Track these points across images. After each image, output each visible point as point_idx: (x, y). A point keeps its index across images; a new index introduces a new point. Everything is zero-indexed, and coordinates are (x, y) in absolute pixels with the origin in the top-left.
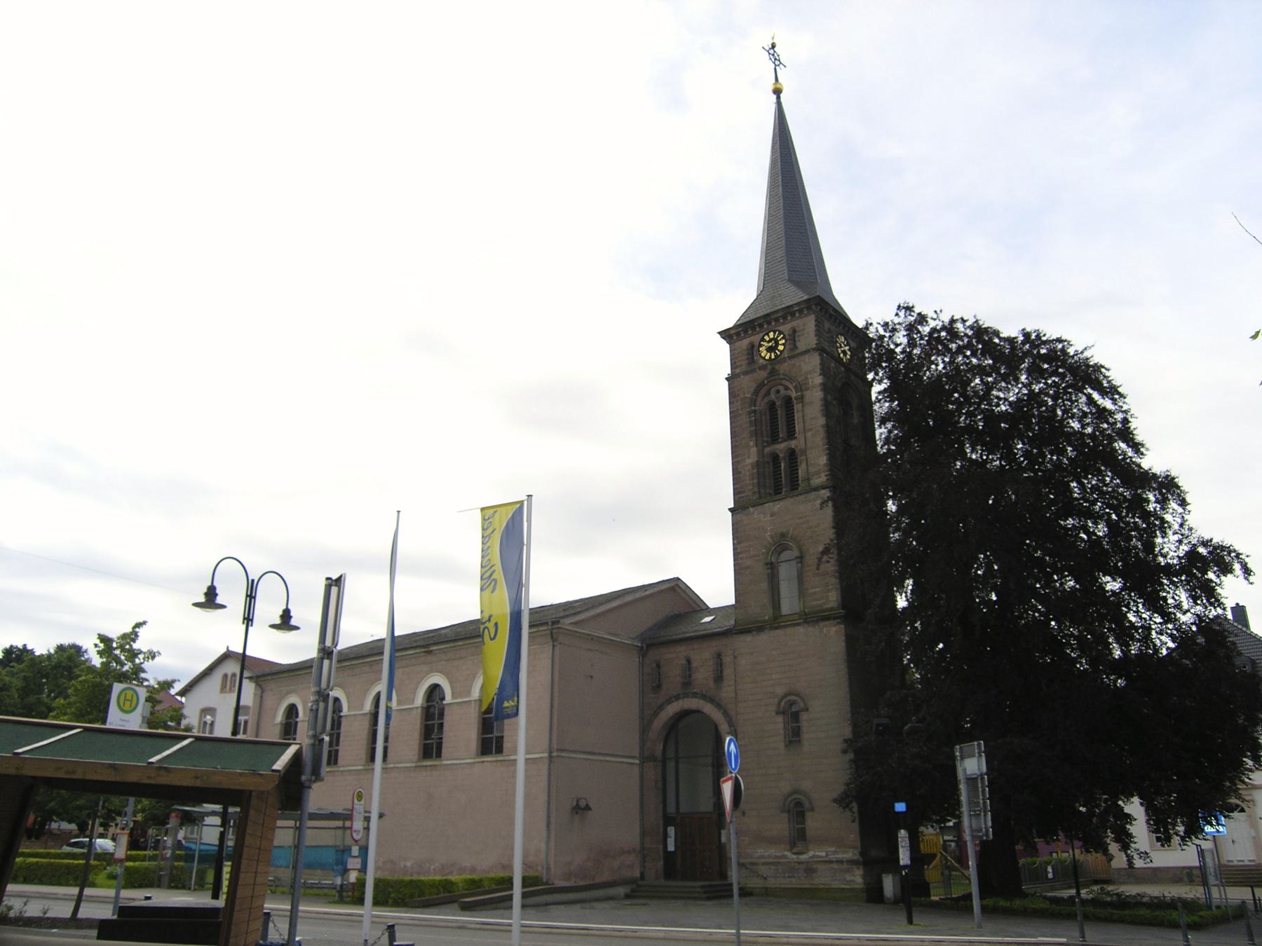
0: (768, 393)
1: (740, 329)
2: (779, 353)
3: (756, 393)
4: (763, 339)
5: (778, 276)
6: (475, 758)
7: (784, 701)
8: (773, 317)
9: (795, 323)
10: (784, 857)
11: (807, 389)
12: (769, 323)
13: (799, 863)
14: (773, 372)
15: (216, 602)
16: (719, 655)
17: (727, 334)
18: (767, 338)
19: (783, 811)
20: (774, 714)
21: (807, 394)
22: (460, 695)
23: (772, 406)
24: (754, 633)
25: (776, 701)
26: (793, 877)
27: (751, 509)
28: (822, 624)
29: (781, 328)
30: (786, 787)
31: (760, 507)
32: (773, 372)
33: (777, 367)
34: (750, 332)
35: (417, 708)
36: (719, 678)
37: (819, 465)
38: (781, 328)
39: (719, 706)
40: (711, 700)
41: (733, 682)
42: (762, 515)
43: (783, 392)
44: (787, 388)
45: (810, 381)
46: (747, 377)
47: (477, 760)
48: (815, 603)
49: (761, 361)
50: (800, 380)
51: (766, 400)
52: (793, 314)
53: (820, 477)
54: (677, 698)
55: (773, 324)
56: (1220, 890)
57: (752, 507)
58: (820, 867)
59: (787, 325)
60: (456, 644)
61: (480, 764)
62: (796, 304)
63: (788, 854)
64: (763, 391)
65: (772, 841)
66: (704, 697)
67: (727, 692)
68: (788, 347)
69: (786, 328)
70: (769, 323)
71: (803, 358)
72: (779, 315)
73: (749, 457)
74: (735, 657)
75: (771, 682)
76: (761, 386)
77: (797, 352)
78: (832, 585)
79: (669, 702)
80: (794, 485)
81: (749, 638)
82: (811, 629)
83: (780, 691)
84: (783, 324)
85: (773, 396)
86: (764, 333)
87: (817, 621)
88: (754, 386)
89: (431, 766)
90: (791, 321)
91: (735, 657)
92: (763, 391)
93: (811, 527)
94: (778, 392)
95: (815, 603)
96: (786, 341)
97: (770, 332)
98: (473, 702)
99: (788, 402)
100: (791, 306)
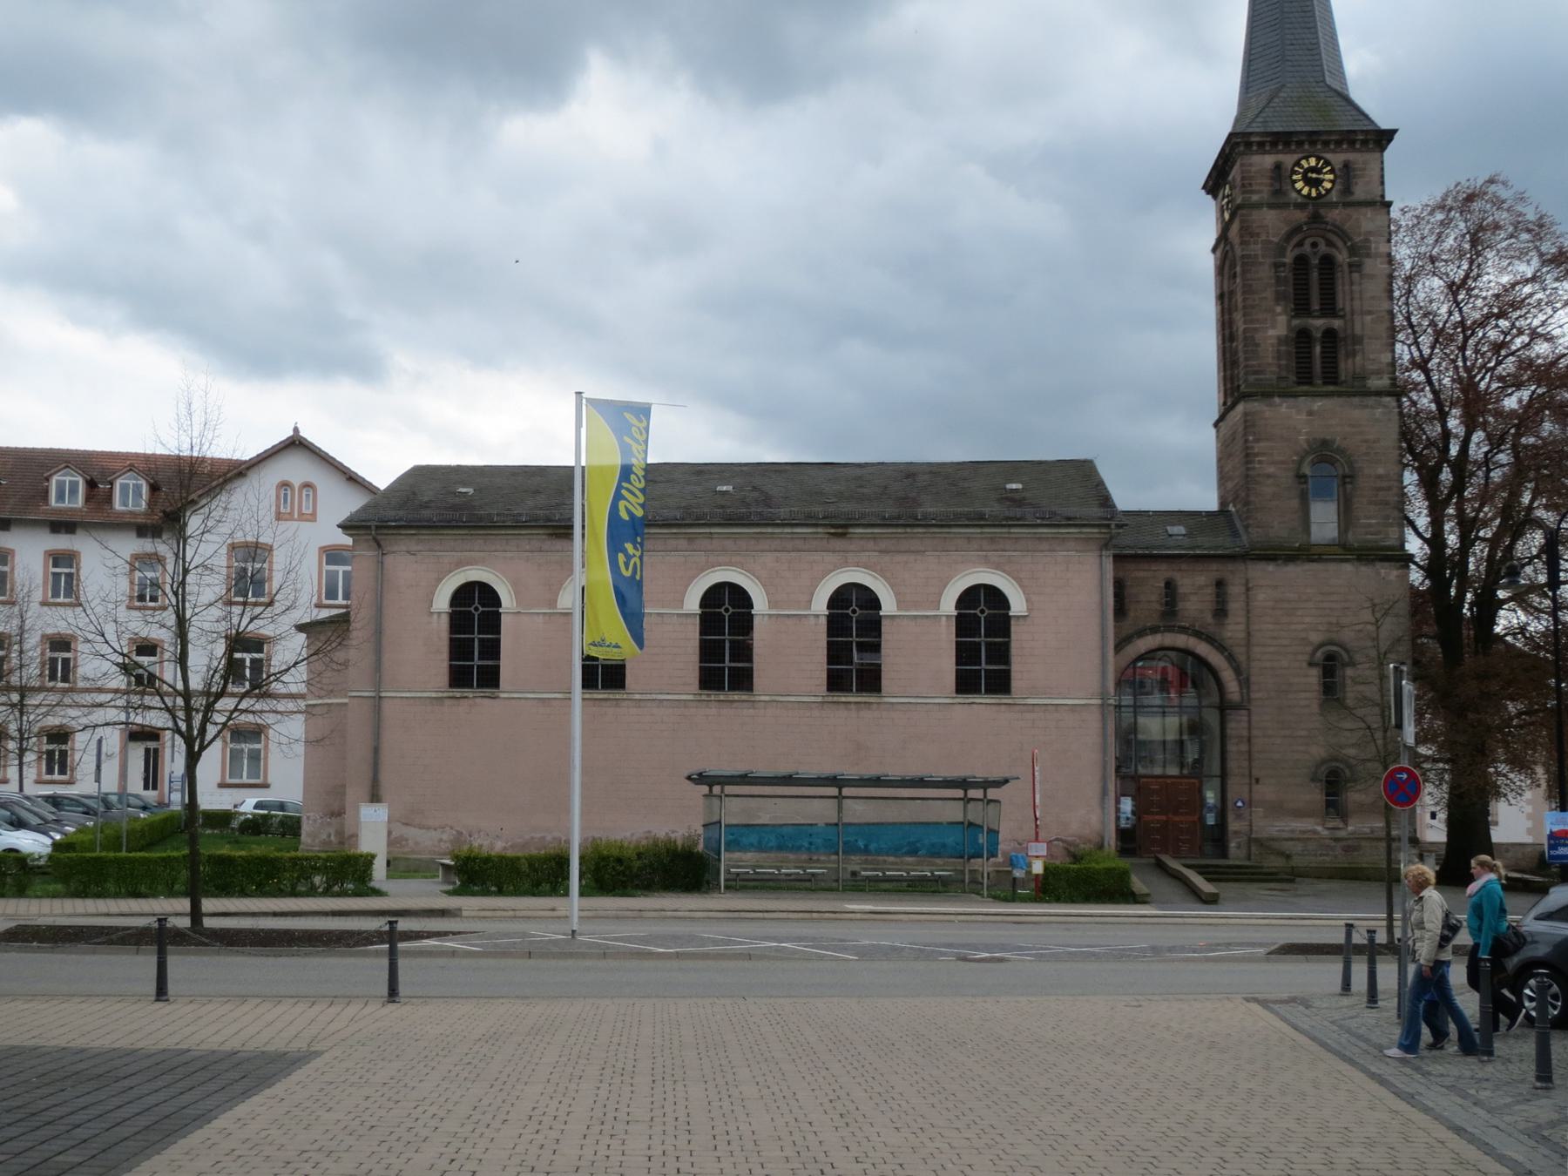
0: (1300, 244)
1: (1269, 139)
2: (1323, 192)
3: (1288, 237)
4: (1298, 164)
5: (1262, 72)
6: (953, 698)
7: (1321, 650)
8: (1324, 138)
9: (1351, 156)
10: (1315, 832)
11: (1368, 255)
12: (1313, 143)
13: (1337, 840)
14: (1316, 218)
15: (1205, 498)
16: (1220, 584)
17: (1246, 139)
18: (1304, 162)
19: (1313, 780)
20: (1305, 665)
21: (1368, 262)
22: (916, 605)
23: (1301, 261)
24: (1280, 562)
25: (1309, 649)
26: (1327, 855)
27: (1277, 400)
28: (1378, 565)
29: (1329, 156)
30: (1318, 751)
31: (1292, 400)
32: (1316, 218)
33: (1322, 211)
34: (1280, 147)
35: (817, 616)
36: (1221, 612)
37: (1381, 363)
38: (1329, 156)
39: (1221, 647)
40: (1210, 640)
41: (1243, 620)
42: (1293, 410)
43: (1323, 248)
44: (1330, 243)
45: (1373, 245)
46: (1273, 212)
47: (830, 699)
48: (1369, 537)
49: (1294, 195)
50: (1357, 239)
51: (1297, 252)
52: (1352, 143)
53: (1381, 378)
54: (1154, 630)
55: (1319, 147)
56: (176, 668)
57: (1279, 396)
58: (1363, 843)
59: (1338, 155)
60: (915, 530)
61: (960, 706)
62: (1362, 131)
63: (1319, 828)
64: (1295, 240)
65: (1299, 814)
66: (1198, 635)
67: (1233, 630)
68: (1338, 187)
69: (1337, 159)
70: (1313, 143)
71: (1363, 210)
72: (1333, 137)
73: (1274, 327)
74: (1248, 589)
75: (1304, 626)
76: (1296, 230)
77: (1351, 199)
78: (1394, 519)
79: (1141, 633)
80: (1331, 376)
81: (1271, 567)
82: (1363, 568)
83: (1316, 638)
84: (1333, 151)
85: (1307, 248)
86: (1300, 155)
87: (1373, 560)
88: (1285, 229)
89: (856, 703)
90: (1346, 151)
91: (1248, 589)
92: (1295, 240)
93: (1366, 441)
94: (1314, 245)
95: (1369, 537)
96: (1335, 177)
97: (1311, 156)
98: (944, 619)
99: (1328, 262)
100: (1354, 132)
